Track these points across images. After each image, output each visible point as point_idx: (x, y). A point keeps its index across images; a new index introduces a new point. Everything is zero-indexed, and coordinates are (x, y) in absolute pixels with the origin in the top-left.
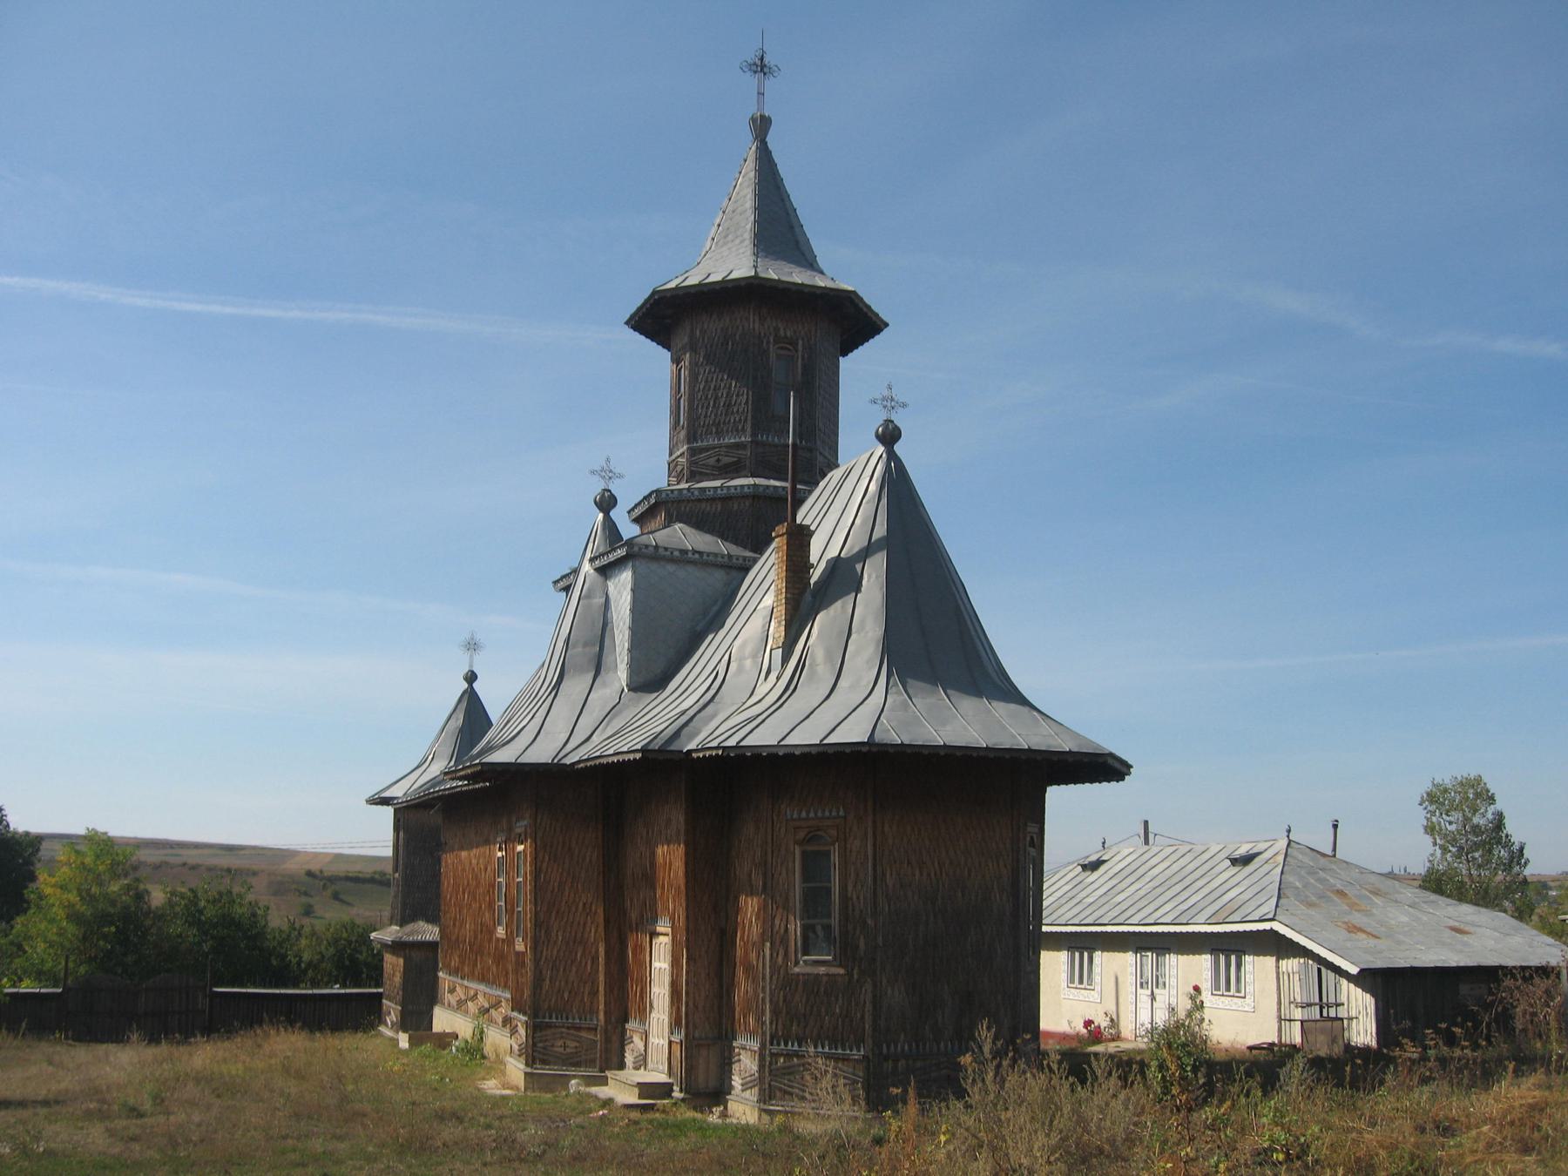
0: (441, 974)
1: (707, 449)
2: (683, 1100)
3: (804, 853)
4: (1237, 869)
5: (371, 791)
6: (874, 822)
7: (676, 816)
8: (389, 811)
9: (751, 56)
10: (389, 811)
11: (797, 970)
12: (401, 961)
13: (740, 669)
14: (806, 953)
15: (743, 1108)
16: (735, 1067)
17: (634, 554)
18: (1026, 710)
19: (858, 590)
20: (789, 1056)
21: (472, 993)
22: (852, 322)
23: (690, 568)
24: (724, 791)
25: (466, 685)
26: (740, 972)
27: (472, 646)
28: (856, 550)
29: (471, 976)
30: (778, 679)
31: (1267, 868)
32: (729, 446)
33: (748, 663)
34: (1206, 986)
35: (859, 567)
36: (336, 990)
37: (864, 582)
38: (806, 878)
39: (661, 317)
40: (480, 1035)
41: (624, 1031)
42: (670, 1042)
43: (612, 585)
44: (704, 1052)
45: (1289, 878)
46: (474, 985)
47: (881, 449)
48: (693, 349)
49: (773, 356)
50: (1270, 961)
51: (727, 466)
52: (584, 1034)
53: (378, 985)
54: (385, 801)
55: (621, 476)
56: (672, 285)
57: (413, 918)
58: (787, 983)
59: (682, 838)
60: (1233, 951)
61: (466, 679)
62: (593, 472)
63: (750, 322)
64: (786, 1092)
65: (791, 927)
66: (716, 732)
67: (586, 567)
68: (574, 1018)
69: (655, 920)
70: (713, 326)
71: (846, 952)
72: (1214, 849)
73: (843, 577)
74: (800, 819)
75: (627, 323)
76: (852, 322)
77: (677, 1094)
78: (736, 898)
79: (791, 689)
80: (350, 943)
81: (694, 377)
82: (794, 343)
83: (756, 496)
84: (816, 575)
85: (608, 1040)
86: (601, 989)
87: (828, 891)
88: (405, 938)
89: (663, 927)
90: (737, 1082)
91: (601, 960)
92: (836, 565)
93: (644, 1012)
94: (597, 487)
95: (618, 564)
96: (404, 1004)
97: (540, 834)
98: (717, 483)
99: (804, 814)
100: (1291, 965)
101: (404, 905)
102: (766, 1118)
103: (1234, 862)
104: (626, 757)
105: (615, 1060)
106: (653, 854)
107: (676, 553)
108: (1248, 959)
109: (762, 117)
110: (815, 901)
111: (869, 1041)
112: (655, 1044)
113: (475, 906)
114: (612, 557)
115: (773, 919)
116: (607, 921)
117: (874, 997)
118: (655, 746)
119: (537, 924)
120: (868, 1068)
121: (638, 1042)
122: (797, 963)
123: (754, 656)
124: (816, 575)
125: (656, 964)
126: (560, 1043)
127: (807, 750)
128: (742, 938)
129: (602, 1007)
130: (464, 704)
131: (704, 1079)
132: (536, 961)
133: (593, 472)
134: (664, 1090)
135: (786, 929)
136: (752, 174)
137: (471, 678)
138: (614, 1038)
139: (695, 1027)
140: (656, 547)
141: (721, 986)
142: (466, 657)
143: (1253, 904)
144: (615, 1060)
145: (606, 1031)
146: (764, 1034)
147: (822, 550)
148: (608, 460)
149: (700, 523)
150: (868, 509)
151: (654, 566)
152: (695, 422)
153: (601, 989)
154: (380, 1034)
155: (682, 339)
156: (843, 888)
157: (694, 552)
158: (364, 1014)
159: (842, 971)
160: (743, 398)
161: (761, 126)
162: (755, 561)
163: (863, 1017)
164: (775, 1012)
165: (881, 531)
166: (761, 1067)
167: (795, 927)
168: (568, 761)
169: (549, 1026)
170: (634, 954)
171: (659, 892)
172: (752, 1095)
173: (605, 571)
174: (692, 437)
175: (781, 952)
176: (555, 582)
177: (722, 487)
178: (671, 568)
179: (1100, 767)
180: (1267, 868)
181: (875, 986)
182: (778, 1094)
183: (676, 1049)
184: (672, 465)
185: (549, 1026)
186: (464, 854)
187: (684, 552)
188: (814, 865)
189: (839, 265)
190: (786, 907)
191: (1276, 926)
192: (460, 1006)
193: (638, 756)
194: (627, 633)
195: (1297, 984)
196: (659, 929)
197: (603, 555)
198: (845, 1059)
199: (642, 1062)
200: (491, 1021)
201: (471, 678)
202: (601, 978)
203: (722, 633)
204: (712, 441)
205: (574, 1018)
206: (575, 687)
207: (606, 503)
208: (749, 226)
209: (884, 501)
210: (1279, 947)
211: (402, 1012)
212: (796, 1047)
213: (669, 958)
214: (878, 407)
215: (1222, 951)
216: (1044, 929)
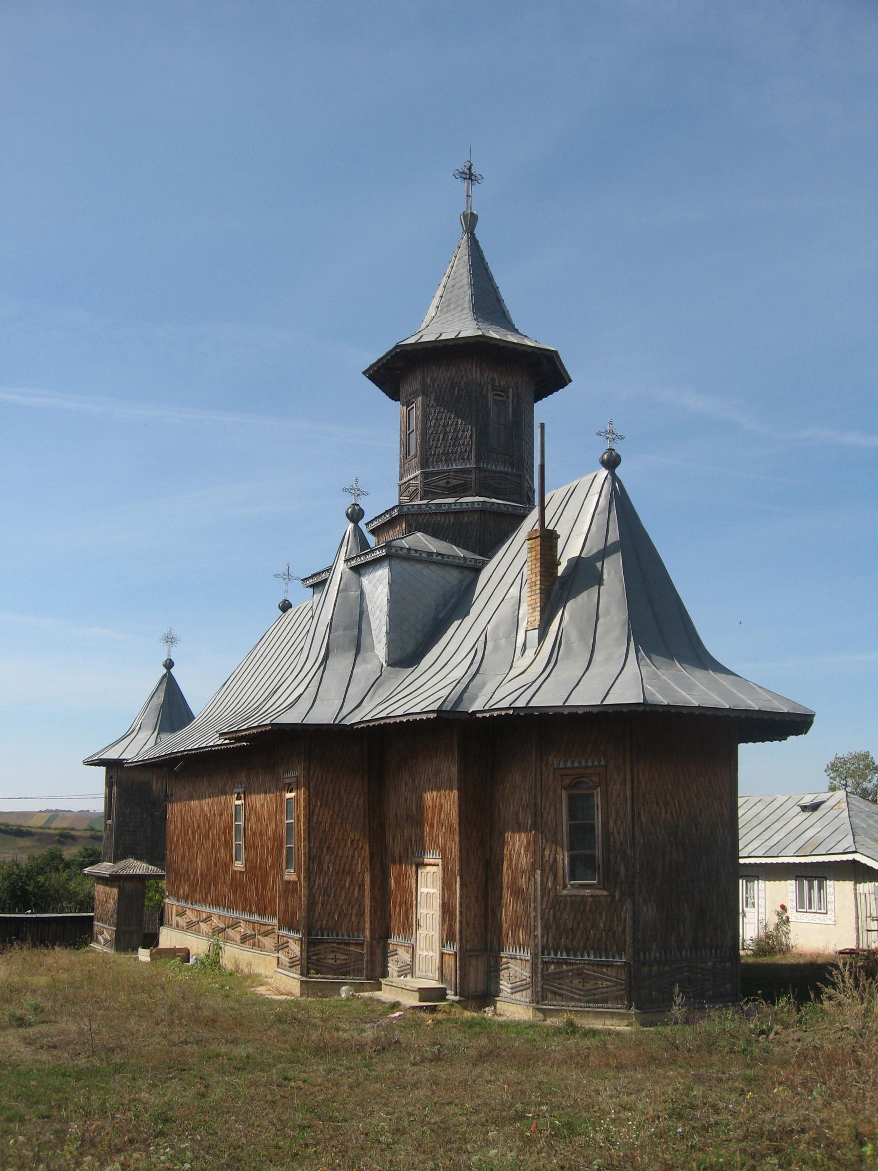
0: (167, 901)
1: (438, 473)
2: (459, 1002)
3: (571, 798)
4: (807, 814)
5: (87, 754)
6: (632, 770)
7: (451, 769)
8: (103, 769)
9: (461, 166)
10: (103, 769)
11: (565, 892)
12: (115, 891)
13: (496, 649)
14: (573, 877)
15: (513, 1007)
16: (504, 974)
17: (392, 555)
18: (466, 695)
19: (600, 582)
20: (559, 963)
21: (204, 916)
22: (545, 373)
23: (433, 568)
24: (486, 747)
25: (165, 671)
26: (507, 896)
27: (170, 640)
28: (594, 551)
29: (204, 901)
30: (537, 654)
31: (834, 813)
32: (457, 471)
33: (503, 642)
34: (791, 905)
35: (599, 565)
36: (29, 914)
37: (605, 576)
38: (572, 815)
39: (393, 373)
40: (217, 950)
41: (386, 946)
42: (442, 955)
43: (365, 581)
44: (474, 962)
45: (857, 821)
46: (206, 909)
47: (604, 473)
48: (425, 393)
49: (490, 399)
50: (849, 885)
51: (455, 487)
52: (352, 948)
53: (92, 912)
54: (100, 763)
55: (367, 494)
56: (412, 341)
57: (124, 857)
58: (555, 903)
59: (455, 783)
60: (816, 878)
61: (165, 666)
62: (345, 490)
63: (474, 373)
64: (555, 993)
65: (559, 857)
66: (495, 695)
67: (341, 566)
68: (344, 935)
69: (423, 851)
70: (442, 376)
71: (609, 879)
72: (781, 799)
73: (585, 573)
74: (566, 768)
75: (364, 373)
76: (545, 373)
77: (451, 996)
78: (502, 835)
79: (552, 660)
80: (21, 877)
81: (426, 416)
82: (506, 392)
83: (483, 511)
84: (561, 570)
85: (372, 953)
86: (367, 911)
87: (592, 828)
88: (120, 872)
89: (432, 857)
90: (505, 986)
91: (367, 887)
92: (576, 563)
93: (409, 927)
94: (347, 502)
95: (376, 562)
96: (118, 925)
97: (312, 784)
98: (452, 500)
99: (569, 764)
100: (866, 887)
101: (117, 845)
102: (540, 1016)
103: (804, 808)
104: (418, 718)
105: (378, 969)
106: (421, 798)
107: (424, 555)
108: (829, 883)
109: (472, 214)
110: (580, 833)
111: (629, 950)
112: (423, 956)
113: (208, 844)
114: (363, 560)
115: (543, 850)
116: (372, 855)
117: (634, 913)
118: (448, 707)
119: (311, 857)
120: (629, 972)
121: (404, 955)
122: (565, 887)
123: (508, 637)
124: (561, 570)
125: (422, 890)
126: (332, 956)
127: (588, 710)
128: (510, 867)
129: (368, 925)
130: (164, 686)
131: (475, 984)
132: (310, 888)
133: (345, 490)
134: (440, 994)
135: (555, 859)
136: (466, 258)
137: (169, 664)
138: (379, 951)
139: (467, 941)
140: (409, 549)
141: (486, 907)
142: (165, 648)
143: (756, 844)
144: (378, 969)
145: (371, 946)
146: (536, 945)
147: (570, 550)
148: (357, 480)
149: (435, 532)
150: (601, 519)
151: (405, 565)
152: (428, 453)
153: (367, 911)
154: (93, 951)
155: (407, 389)
156: (605, 824)
157: (438, 554)
158: (78, 933)
159: (605, 893)
160: (468, 434)
161: (471, 221)
162: (484, 564)
163: (624, 931)
164: (546, 927)
165: (614, 536)
166: (534, 972)
167: (563, 858)
168: (348, 722)
169: (322, 942)
170: (397, 881)
171: (427, 829)
172: (525, 996)
173: (358, 570)
174: (424, 463)
175: (551, 878)
176: (304, 580)
177: (427, 505)
178: (419, 566)
179: (794, 724)
180: (834, 813)
181: (634, 903)
182: (549, 995)
183: (450, 962)
184: (404, 488)
185: (322, 942)
186: (194, 803)
187: (430, 554)
188: (579, 807)
189: (532, 330)
190: (556, 842)
191: (858, 857)
192: (191, 926)
193: (432, 716)
194: (384, 619)
195: (873, 902)
196: (426, 861)
197: (352, 559)
198: (609, 965)
199: (409, 970)
200: (227, 939)
201: (169, 664)
202: (367, 902)
203: (469, 620)
204: (442, 467)
205: (344, 935)
206: (340, 664)
207: (355, 515)
208: (467, 298)
209: (614, 512)
210: (856, 872)
211: (116, 931)
212: (565, 957)
213: (439, 884)
214: (602, 438)
215: (806, 877)
216: (741, 861)
